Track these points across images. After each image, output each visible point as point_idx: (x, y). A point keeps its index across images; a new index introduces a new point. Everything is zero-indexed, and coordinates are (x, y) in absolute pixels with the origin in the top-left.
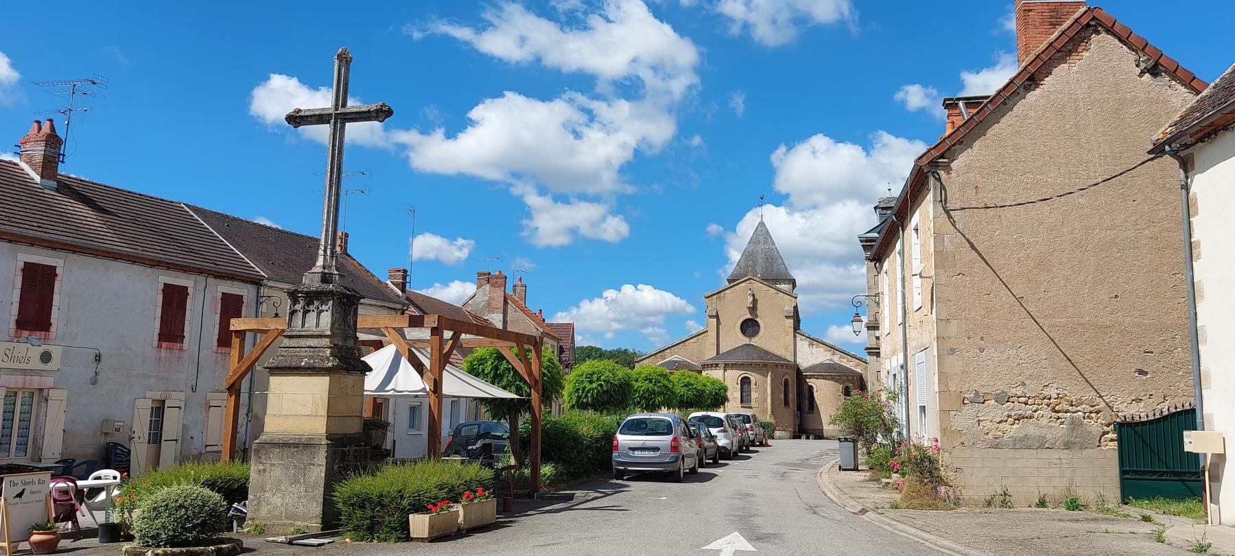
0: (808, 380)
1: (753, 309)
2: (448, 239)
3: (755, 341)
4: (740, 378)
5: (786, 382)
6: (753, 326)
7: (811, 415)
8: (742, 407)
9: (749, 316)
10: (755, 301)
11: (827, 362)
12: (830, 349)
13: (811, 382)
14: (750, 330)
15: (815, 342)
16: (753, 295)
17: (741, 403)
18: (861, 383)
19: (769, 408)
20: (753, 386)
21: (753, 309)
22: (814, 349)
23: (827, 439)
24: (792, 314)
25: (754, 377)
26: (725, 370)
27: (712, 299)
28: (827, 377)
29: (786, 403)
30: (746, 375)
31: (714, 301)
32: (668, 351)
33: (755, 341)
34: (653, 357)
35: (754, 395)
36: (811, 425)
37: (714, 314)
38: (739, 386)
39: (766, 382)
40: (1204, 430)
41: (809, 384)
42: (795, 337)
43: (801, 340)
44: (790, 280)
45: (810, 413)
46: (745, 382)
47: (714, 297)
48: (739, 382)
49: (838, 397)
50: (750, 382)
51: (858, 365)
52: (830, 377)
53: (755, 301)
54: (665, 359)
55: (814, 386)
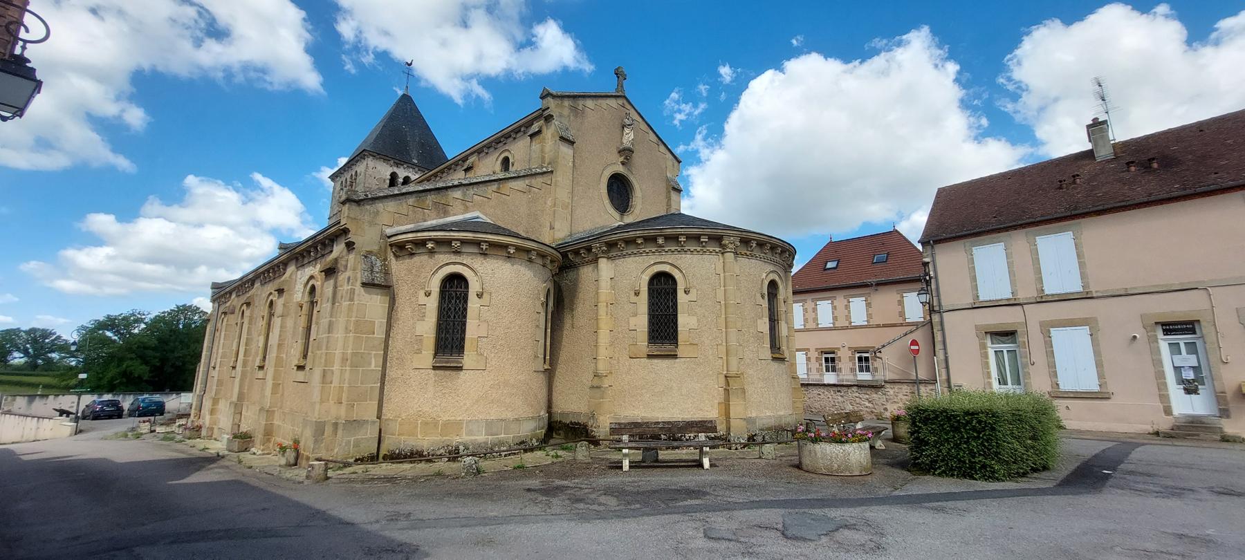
54: (446, 214)
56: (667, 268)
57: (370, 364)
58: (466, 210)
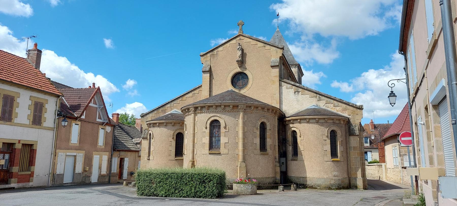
0: (291, 125)
1: (242, 62)
2: (7, 27)
3: (244, 92)
4: (209, 122)
5: (263, 127)
6: (243, 78)
7: (295, 162)
8: (210, 154)
9: (238, 70)
10: (243, 55)
11: (313, 107)
12: (315, 95)
13: (295, 127)
14: (240, 83)
15: (300, 90)
16: (242, 50)
17: (210, 149)
18: (349, 127)
19: (241, 154)
20: (222, 130)
21: (242, 62)
22: (300, 96)
23: (312, 187)
24: (277, 64)
25: (223, 119)
26: (195, 114)
27: (207, 57)
28: (311, 121)
29: (263, 147)
30: (215, 118)
31: (209, 58)
32: (169, 105)
33: (244, 92)
34: (155, 112)
35: (223, 140)
36: (294, 173)
37: (208, 69)
38: (208, 131)
39: (237, 125)
40: (416, 167)
41: (293, 129)
42: (280, 85)
43: (287, 88)
44: (296, 65)
45: (294, 160)
46: (215, 125)
47: (209, 55)
48: (208, 126)
49: (324, 142)
50: (220, 126)
51: (344, 110)
52: (314, 121)
53: (243, 55)
54: (165, 113)
55: (298, 131)
56: (217, 118)
57: (145, 159)
58: (172, 110)
